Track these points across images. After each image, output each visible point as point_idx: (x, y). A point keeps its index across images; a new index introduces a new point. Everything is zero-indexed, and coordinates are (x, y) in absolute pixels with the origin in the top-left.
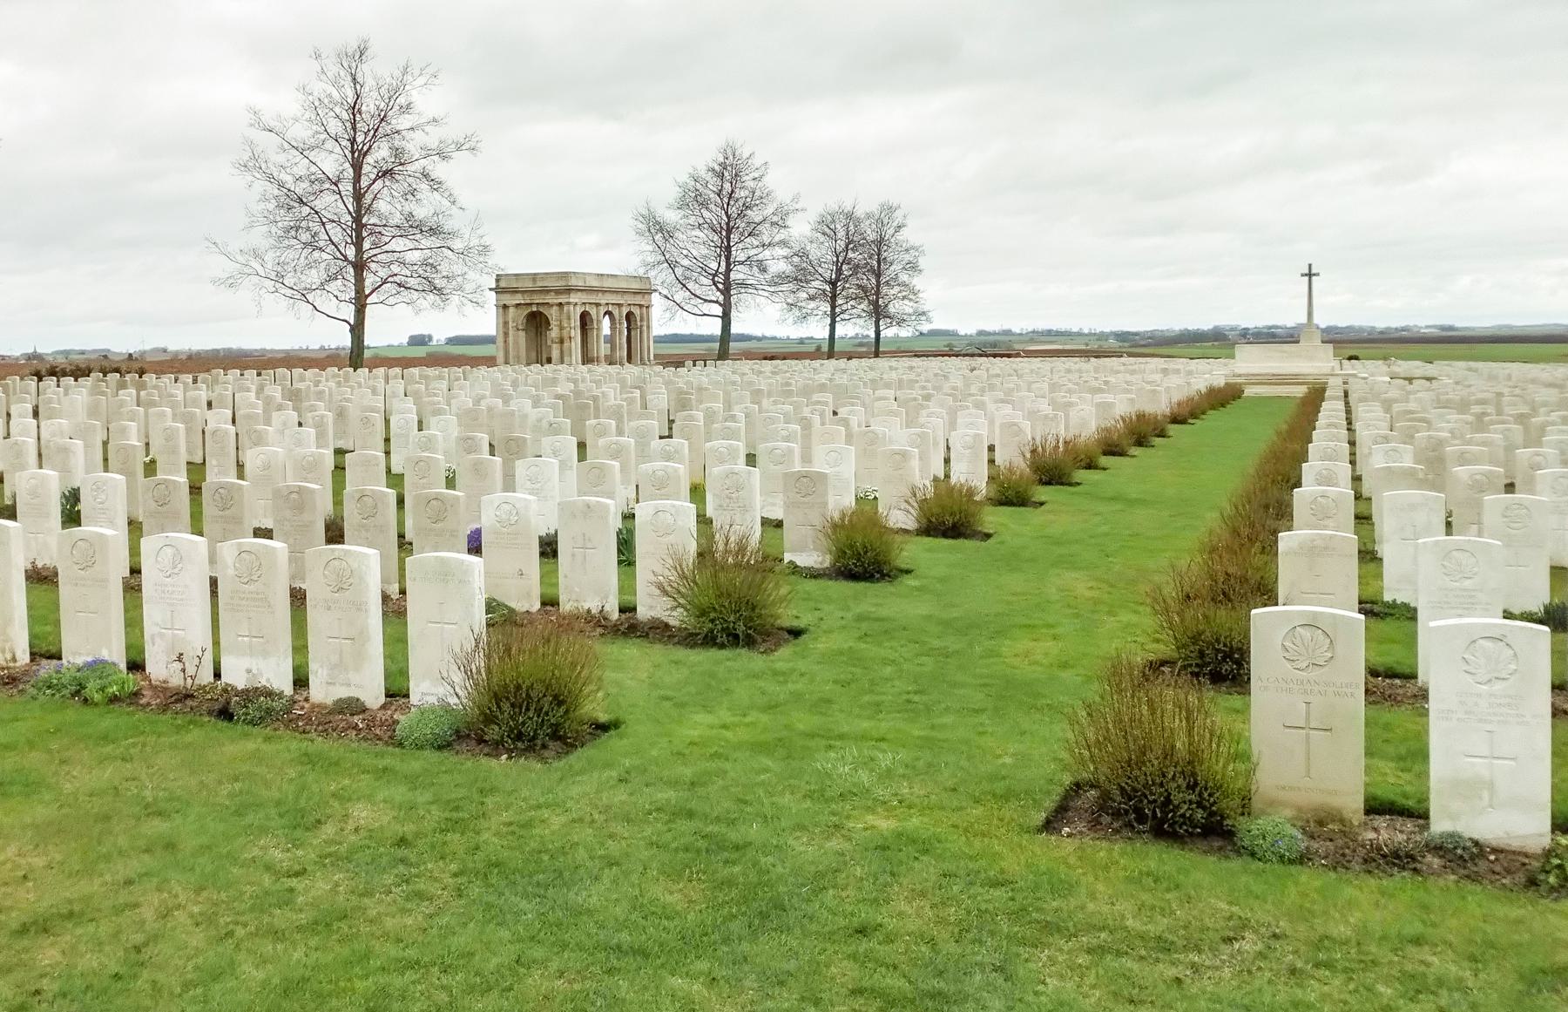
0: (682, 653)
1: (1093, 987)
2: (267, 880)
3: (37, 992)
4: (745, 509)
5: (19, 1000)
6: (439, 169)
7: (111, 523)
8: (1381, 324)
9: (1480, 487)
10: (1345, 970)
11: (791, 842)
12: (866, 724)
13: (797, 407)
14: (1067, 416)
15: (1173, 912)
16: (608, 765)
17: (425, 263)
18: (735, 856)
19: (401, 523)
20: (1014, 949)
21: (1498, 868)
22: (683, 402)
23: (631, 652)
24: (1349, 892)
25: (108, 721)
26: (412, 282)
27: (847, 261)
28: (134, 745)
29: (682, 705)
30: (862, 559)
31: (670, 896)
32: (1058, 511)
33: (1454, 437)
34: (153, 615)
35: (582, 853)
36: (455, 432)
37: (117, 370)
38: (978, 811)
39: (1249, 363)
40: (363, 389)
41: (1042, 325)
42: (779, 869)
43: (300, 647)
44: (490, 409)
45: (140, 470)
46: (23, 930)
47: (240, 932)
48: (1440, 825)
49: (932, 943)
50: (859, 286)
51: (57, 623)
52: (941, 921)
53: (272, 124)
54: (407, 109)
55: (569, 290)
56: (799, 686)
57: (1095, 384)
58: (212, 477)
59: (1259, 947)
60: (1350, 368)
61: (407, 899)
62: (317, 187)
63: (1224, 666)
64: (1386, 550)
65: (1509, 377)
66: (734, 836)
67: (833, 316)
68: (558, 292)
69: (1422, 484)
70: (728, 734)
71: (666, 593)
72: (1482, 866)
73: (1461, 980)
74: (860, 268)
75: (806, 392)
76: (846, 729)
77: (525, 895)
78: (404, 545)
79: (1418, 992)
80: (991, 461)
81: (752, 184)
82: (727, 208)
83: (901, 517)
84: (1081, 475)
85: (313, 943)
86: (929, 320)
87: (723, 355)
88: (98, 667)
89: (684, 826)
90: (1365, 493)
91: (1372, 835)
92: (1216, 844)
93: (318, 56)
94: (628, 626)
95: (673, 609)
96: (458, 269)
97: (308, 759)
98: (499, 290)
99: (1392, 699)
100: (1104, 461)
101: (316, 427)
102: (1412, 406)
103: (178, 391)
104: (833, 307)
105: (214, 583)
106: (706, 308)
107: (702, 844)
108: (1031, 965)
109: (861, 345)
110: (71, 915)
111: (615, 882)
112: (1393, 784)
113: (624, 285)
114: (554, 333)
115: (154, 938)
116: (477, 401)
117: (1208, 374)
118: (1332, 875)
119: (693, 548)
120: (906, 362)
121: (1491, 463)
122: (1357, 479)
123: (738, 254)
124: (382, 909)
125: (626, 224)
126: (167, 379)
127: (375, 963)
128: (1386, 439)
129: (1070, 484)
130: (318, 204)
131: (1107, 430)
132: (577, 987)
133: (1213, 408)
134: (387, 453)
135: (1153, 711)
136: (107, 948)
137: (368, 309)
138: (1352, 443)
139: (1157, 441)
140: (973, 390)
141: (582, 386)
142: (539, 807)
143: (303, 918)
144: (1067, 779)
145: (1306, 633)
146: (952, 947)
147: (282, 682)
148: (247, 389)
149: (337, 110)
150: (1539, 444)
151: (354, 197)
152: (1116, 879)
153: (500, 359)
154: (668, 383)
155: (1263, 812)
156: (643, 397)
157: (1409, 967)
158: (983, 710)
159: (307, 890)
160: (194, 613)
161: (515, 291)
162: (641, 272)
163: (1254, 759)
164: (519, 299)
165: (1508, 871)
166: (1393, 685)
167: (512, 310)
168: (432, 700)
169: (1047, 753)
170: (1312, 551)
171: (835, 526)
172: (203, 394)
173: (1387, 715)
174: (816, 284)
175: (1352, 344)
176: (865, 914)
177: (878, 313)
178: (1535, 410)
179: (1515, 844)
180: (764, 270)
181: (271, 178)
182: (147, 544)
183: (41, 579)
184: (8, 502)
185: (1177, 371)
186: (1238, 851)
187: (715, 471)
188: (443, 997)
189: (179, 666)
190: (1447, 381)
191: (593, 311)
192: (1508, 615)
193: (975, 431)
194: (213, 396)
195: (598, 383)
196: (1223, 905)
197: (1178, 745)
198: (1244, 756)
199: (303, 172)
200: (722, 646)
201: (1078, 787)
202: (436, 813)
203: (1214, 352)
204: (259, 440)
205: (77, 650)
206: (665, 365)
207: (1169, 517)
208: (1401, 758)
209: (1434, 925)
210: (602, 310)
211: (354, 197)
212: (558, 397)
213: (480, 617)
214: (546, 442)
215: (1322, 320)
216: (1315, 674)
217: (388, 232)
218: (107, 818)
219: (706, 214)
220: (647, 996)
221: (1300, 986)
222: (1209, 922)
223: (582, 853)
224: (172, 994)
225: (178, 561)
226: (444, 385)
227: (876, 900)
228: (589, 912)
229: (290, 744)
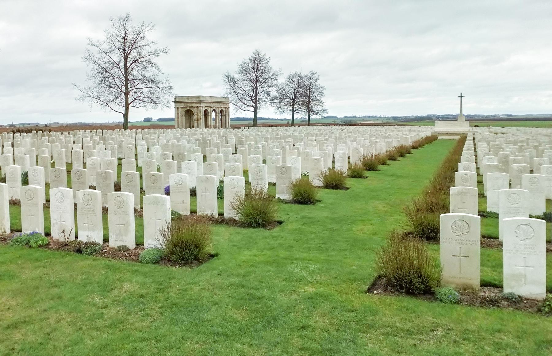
0: (240, 230)
1: (385, 347)
2: (94, 309)
3: (13, 349)
4: (262, 179)
5: (7, 352)
6: (155, 60)
7: (39, 184)
8: (486, 114)
9: (521, 171)
10: (474, 341)
12: (305, 255)
13: (281, 143)
14: (376, 146)
15: (413, 321)
16: (214, 269)
17: (150, 93)
18: (259, 301)
19: (141, 184)
20: (357, 334)
21: (527, 305)
23: (222, 229)
24: (475, 314)
25: (38, 254)
26: (145, 99)
27: (298, 92)
28: (47, 262)
29: (240, 248)
30: (303, 197)
31: (236, 315)
33: (512, 154)
35: (205, 301)
36: (160, 152)
37: (41, 130)
38: (344, 285)
39: (440, 127)
40: (128, 137)
42: (274, 306)
43: (106, 228)
44: (172, 144)
45: (49, 165)
46: (8, 327)
47: (85, 328)
48: (507, 290)
49: (328, 332)
50: (302, 101)
51: (20, 219)
52: (331, 324)
53: (96, 44)
54: (143, 38)
55: (200, 102)
56: (281, 241)
57: (385, 135)
59: (443, 333)
60: (475, 129)
61: (143, 316)
62: (111, 66)
63: (431, 234)
64: (488, 194)
65: (531, 133)
66: (258, 294)
67: (293, 111)
68: (196, 103)
69: (501, 170)
70: (256, 258)
71: (234, 209)
72: (522, 304)
73: (514, 345)
74: (303, 94)
75: (284, 138)
76: (298, 256)
77: (185, 315)
78: (142, 192)
79: (499, 349)
80: (349, 162)
81: (265, 65)
82: (256, 73)
83: (317, 182)
84: (380, 167)
85: (110, 332)
86: (327, 113)
87: (255, 125)
88: (34, 234)
89: (241, 290)
90: (481, 173)
91: (483, 294)
92: (428, 297)
93: (112, 20)
94: (221, 220)
95: (237, 214)
96: (161, 95)
97: (109, 267)
98: (176, 102)
99: (491, 246)
100: (389, 162)
102: (497, 143)
103: (63, 138)
104: (293, 108)
105: (75, 205)
106: (249, 108)
107: (247, 297)
108: (363, 340)
109: (303, 121)
110: (25, 322)
111: (216, 310)
112: (490, 276)
113: (219, 100)
114: (195, 117)
115: (55, 330)
116: (168, 141)
117: (425, 132)
118: (469, 308)
119: (244, 193)
121: (525, 163)
122: (478, 168)
123: (260, 89)
124: (134, 320)
125: (221, 78)
126: (59, 133)
128: (488, 155)
129: (377, 170)
130: (112, 72)
131: (390, 151)
132: (203, 347)
133: (427, 143)
134: (136, 159)
136: (38, 334)
137: (130, 109)
138: (476, 156)
140: (343, 137)
141: (205, 136)
142: (190, 284)
143: (107, 323)
144: (376, 274)
145: (460, 223)
147: (99, 240)
148: (87, 137)
149: (119, 39)
150: (542, 156)
151: (125, 70)
152: (393, 309)
153: (176, 126)
154: (235, 135)
155: (445, 286)
156: (226, 140)
157: (496, 340)
158: (346, 250)
159: (108, 313)
160: (68, 216)
161: (181, 102)
162: (226, 96)
163: (442, 267)
164: (183, 105)
165: (531, 307)
166: (491, 241)
167: (180, 109)
168: (152, 246)
169: (369, 265)
170: (462, 194)
171: (294, 185)
173: (488, 251)
174: (287, 100)
175: (476, 121)
176: (305, 322)
177: (309, 110)
178: (540, 144)
179: (533, 297)
180: (269, 95)
181: (95, 63)
182: (52, 191)
183: (15, 204)
184: (3, 177)
185: (414, 131)
186: (436, 300)
187: (252, 166)
188: (156, 351)
189: (63, 234)
190: (509, 134)
191: (209, 110)
192: (531, 216)
193: (343, 152)
194: (75, 139)
197: (415, 262)
198: (438, 266)
199: (107, 61)
200: (254, 227)
201: (379, 277)
203: (422, 124)
204: (91, 155)
205: (27, 228)
206: (234, 128)
207: (412, 182)
208: (493, 267)
209: (505, 325)
210: (212, 109)
211: (125, 70)
212: (196, 140)
213: (169, 217)
214: (192, 155)
215: (466, 112)
216: (463, 237)
217: (136, 82)
218: (38, 288)
219: (249, 75)
221: (458, 347)
222: (425, 324)
225: (63, 197)
226: (156, 135)
227: (308, 317)
228: (208, 321)
229: (102, 262)
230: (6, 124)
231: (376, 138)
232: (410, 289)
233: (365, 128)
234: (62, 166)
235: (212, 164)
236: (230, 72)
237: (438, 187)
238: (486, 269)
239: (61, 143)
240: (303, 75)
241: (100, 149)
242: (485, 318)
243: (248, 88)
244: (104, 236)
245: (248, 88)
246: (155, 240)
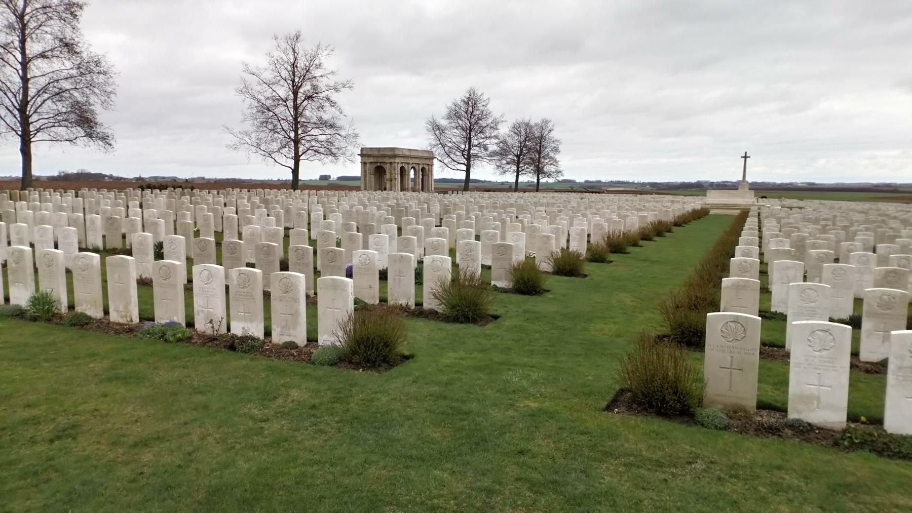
0: (443, 325)
1: (626, 481)
2: (251, 423)
3: (142, 473)
4: (474, 260)
5: (133, 477)
6: (334, 96)
7: (178, 259)
8: (778, 181)
9: (822, 259)
10: (744, 479)
11: (490, 411)
12: (526, 360)
13: (500, 214)
14: (625, 221)
15: (664, 449)
16: (408, 375)
17: (327, 141)
18: (465, 417)
19: (315, 262)
20: (590, 463)
21: (820, 437)
22: (446, 210)
23: (420, 324)
24: (747, 444)
25: (176, 350)
26: (322, 150)
27: (525, 146)
28: (189, 361)
29: (442, 348)
30: (527, 283)
31: (434, 434)
32: (619, 265)
33: (811, 236)
34: (198, 302)
35: (395, 414)
36: (341, 221)
37: (180, 187)
38: (576, 400)
39: (713, 198)
40: (298, 200)
41: (615, 179)
42: (485, 423)
43: (268, 318)
44: (357, 211)
45: (192, 234)
46: (135, 445)
47: (238, 446)
48: (792, 415)
49: (553, 459)
50: (531, 158)
51: (152, 305)
52: (558, 449)
53: (254, 71)
54: (319, 66)
55: (395, 156)
56: (496, 341)
57: (639, 207)
58: (227, 238)
59: (704, 467)
60: (762, 202)
61: (315, 433)
62: (276, 103)
63: (693, 338)
64: (774, 288)
65: (841, 208)
66: (464, 408)
67: (518, 172)
68: (390, 157)
69: (793, 257)
70: (464, 362)
71: (436, 298)
72: (812, 435)
73: (800, 487)
74: (531, 148)
75: (504, 207)
76: (517, 361)
77: (369, 432)
78: (317, 273)
79: (779, 491)
80: (589, 242)
81: (482, 108)
82: (470, 118)
83: (546, 266)
84: (630, 249)
85: (271, 452)
86: (562, 175)
87: (466, 189)
88: (172, 325)
89: (443, 403)
90: (765, 260)
91: (759, 419)
93: (276, 38)
94: (419, 312)
95: (440, 305)
96: (343, 144)
97: (270, 369)
98: (362, 155)
99: (772, 357)
100: (641, 243)
101: (276, 216)
102: (791, 220)
103: (210, 198)
104: (518, 168)
105: (227, 287)
106: (459, 167)
107: (450, 411)
108: (598, 471)
109: (530, 186)
110: (158, 438)
111: (410, 427)
112: (771, 395)
113: (421, 155)
114: (388, 176)
115: (197, 449)
116: (351, 207)
117: (693, 203)
118: (740, 436)
119: (449, 277)
120: (551, 194)
121: (828, 248)
122: (761, 255)
123: (475, 141)
124: (303, 437)
125: (423, 125)
126: (205, 192)
127: (300, 461)
128: (777, 236)
129: (625, 253)
130: (277, 111)
131: (644, 228)
132: (391, 474)
134: (309, 230)
135: (658, 358)
136: (175, 454)
137: (301, 162)
138: (760, 237)
140: (582, 208)
141: (400, 202)
142: (376, 393)
143: (267, 441)
144: (618, 387)
146: (562, 461)
147: (259, 333)
148: (244, 199)
149: (286, 65)
150: (853, 240)
151: (294, 109)
152: (638, 433)
153: (362, 187)
154: (440, 201)
156: (428, 207)
157: (775, 480)
158: (580, 355)
159: (269, 428)
160: (216, 300)
161: (369, 156)
162: (429, 148)
163: (705, 381)
164: (371, 160)
165: (825, 438)
166: (774, 350)
168: (329, 343)
169: (609, 375)
170: (738, 287)
171: (515, 269)
172: (222, 200)
173: (769, 364)
174: (510, 156)
175: (763, 190)
176: (523, 445)
177: (539, 171)
178: (852, 224)
179: (829, 426)
180: (486, 149)
181: (254, 97)
182: (196, 269)
183: (144, 284)
184: (128, 247)
185: (678, 202)
186: (696, 423)
187: (461, 242)
188: (331, 477)
189: (210, 325)
190: (809, 209)
191: (406, 167)
192: (831, 320)
193: (579, 228)
194: (227, 201)
195: (408, 200)
196: (688, 447)
197: (670, 374)
198: (700, 380)
199: (269, 95)
200: (462, 323)
201: (622, 391)
202: (329, 394)
204: (249, 222)
205: (162, 316)
207: (672, 270)
208: (775, 384)
209: (787, 461)
210: (410, 166)
211: (294, 109)
212: (389, 206)
213: (351, 306)
214: (383, 226)
215: (749, 179)
216: (736, 344)
217: (310, 126)
218: (176, 394)
219: (460, 122)
220: (423, 479)
221: (722, 485)
222: (681, 455)
223: (395, 414)
224: (205, 474)
225: (210, 277)
226: (336, 199)
227: (528, 439)
228: (398, 440)
229: (262, 362)
230: (131, 176)
231: (627, 210)
232: (662, 407)
233: (612, 196)
234: (209, 236)
235: (408, 239)
236: (435, 117)
237: (706, 277)
238: (765, 386)
239: (208, 204)
240: (532, 123)
241: (261, 215)
243: (459, 140)
244: (265, 328)
245: (459, 140)
246: (331, 336)
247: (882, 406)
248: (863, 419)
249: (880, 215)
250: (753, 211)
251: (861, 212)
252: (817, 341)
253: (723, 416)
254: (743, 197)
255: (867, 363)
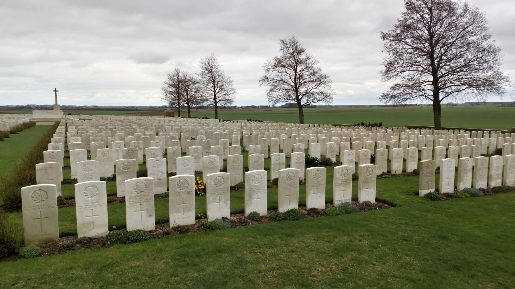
8: (78, 105)
21: (96, 243)
39: (37, 115)
48: (80, 236)
59: (24, 284)
60: (68, 117)
72: (91, 244)
86: (498, 91)
91: (61, 243)
92: (13, 257)
102: (84, 127)
112: (68, 227)
117: (25, 119)
118: (48, 257)
128: (75, 136)
133: (25, 129)
139: (6, 139)
145: (39, 192)
155: (28, 245)
165: (98, 243)
166: (67, 202)
173: (63, 209)
175: (69, 110)
179: (100, 236)
185: (14, 118)
198: (23, 230)
203: (23, 112)
215: (61, 103)
216: (42, 203)
222: (7, 281)
242: (61, 262)
247: (125, 219)
248: (114, 227)
249: (129, 122)
250: (63, 122)
251: (120, 121)
252: (89, 192)
253: (38, 248)
254: (56, 114)
255: (121, 197)
